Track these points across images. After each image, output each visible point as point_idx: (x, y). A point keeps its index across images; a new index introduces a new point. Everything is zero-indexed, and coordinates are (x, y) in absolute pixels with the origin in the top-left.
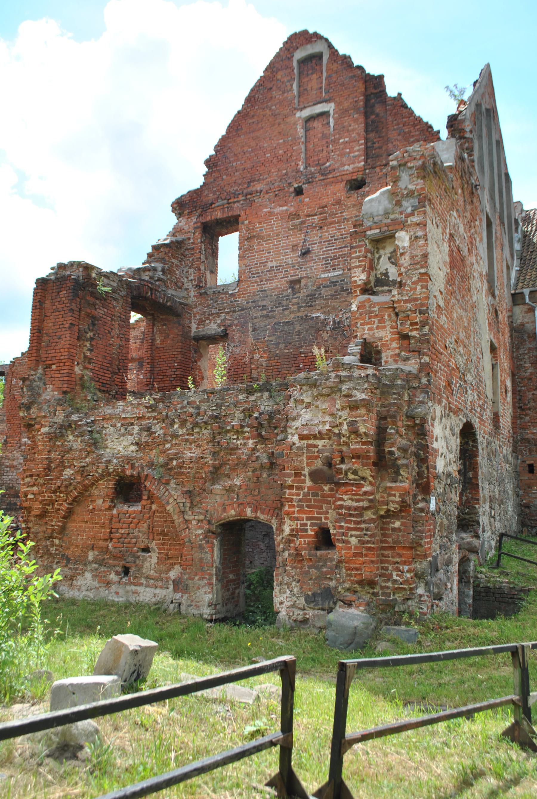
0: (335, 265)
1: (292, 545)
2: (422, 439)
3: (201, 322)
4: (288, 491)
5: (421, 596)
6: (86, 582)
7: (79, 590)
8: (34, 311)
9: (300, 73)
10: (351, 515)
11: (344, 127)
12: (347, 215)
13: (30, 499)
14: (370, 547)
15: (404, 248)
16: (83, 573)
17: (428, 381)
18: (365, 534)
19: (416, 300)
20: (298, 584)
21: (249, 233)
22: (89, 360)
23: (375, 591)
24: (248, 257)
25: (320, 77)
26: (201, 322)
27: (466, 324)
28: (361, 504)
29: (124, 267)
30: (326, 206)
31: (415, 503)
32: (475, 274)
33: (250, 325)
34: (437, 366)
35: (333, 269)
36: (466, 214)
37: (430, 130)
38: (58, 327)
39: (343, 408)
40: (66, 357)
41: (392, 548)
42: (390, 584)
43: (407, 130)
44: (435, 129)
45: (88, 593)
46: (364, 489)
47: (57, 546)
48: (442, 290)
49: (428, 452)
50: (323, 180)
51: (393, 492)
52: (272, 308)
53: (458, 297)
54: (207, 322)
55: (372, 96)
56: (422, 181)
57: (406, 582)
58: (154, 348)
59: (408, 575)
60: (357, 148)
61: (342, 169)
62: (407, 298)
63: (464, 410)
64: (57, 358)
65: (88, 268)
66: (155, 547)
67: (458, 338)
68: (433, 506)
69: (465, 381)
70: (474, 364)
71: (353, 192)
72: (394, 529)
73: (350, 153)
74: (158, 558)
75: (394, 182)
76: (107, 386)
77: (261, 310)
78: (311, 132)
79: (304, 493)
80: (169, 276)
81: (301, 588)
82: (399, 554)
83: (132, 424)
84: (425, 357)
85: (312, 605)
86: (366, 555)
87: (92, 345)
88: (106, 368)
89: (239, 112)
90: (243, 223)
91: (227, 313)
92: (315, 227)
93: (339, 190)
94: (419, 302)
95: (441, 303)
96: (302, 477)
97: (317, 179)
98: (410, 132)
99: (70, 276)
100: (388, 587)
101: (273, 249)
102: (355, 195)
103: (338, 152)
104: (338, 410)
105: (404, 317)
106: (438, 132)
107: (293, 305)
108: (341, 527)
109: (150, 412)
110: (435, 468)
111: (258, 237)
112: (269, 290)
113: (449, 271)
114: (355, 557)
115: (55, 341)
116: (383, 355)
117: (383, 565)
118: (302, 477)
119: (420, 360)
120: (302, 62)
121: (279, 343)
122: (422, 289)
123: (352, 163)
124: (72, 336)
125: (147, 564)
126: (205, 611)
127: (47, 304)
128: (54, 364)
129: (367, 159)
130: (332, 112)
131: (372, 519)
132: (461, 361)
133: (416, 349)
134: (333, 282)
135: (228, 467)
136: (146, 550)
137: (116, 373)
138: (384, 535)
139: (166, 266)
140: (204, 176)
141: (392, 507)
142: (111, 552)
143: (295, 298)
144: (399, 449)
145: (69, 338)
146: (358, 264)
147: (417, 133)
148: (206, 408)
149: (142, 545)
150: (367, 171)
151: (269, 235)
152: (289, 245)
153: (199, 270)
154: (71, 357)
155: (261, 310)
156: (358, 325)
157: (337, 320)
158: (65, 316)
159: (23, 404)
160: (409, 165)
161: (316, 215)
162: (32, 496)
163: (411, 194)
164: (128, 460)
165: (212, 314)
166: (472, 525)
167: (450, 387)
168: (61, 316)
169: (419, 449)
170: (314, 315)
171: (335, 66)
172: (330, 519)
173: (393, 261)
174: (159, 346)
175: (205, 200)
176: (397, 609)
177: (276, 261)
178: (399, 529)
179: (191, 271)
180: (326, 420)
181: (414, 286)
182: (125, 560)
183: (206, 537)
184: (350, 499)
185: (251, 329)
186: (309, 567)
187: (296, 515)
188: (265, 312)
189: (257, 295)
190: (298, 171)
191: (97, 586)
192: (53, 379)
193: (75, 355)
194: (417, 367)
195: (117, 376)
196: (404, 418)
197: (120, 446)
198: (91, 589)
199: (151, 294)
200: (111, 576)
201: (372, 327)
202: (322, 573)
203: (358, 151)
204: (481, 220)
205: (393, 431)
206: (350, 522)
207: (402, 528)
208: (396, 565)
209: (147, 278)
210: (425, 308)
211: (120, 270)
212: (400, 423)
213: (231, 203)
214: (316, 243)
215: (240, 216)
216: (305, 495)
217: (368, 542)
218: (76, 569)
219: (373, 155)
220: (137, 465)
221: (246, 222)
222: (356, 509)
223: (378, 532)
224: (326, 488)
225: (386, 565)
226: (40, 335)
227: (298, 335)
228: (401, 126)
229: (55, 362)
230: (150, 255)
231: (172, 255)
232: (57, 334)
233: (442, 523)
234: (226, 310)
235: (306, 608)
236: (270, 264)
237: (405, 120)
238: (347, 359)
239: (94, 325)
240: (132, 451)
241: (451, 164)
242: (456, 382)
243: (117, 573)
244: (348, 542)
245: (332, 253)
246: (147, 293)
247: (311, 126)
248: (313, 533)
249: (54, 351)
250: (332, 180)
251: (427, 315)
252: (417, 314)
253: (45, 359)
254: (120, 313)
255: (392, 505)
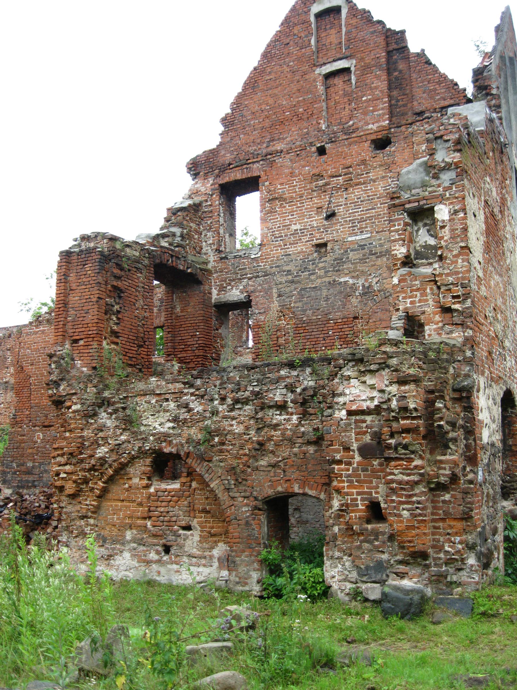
0: (362, 228)
1: (341, 520)
2: (469, 412)
3: (222, 289)
4: (336, 467)
5: (472, 566)
6: (124, 561)
7: (117, 570)
8: (59, 285)
9: (318, 28)
10: (402, 489)
11: (366, 85)
12: (373, 176)
13: (63, 478)
14: (422, 520)
15: (443, 221)
16: (121, 552)
17: (473, 354)
18: (417, 508)
19: (457, 273)
20: (349, 558)
21: (270, 195)
22: (115, 334)
23: (427, 562)
24: (270, 220)
25: (340, 31)
26: (222, 289)
27: (502, 290)
28: (412, 478)
29: (142, 234)
30: (350, 167)
31: (465, 475)
32: (507, 236)
33: (275, 290)
34: (480, 337)
35: (361, 232)
36: (497, 177)
37: (456, 87)
38: (85, 301)
39: (391, 384)
40: (95, 332)
41: (443, 520)
42: (442, 555)
43: (432, 88)
44: (461, 87)
45: (127, 573)
46: (414, 464)
47: (92, 525)
48: (481, 260)
49: (475, 425)
50: (347, 139)
51: (443, 466)
52: (297, 273)
53: (494, 264)
54: (228, 288)
55: (394, 52)
56: (459, 154)
57: (458, 552)
58: (174, 317)
59: (460, 546)
60: (381, 106)
61: (366, 127)
62: (449, 271)
63: (504, 377)
64: (85, 333)
65: (113, 239)
66: (197, 526)
67: (496, 305)
68: (480, 477)
69: (504, 348)
70: (510, 329)
71: (378, 152)
72: (444, 502)
73: (373, 111)
74: (201, 535)
75: (431, 155)
76: (134, 359)
77: (286, 275)
78: (332, 89)
79: (353, 468)
80: (187, 242)
81: (353, 562)
82: (450, 526)
83: (167, 400)
84: (468, 330)
85: (364, 579)
86: (418, 528)
87: (118, 319)
88: (132, 341)
89: (255, 69)
90: (264, 185)
91: (250, 279)
92: (340, 188)
93: (365, 150)
94: (460, 276)
95: (481, 274)
96: (351, 453)
97: (340, 139)
98: (435, 89)
99: (95, 248)
100: (440, 559)
101: (296, 211)
102: (380, 154)
103: (361, 111)
104: (387, 386)
105: (447, 290)
106: (465, 90)
107: (319, 269)
108: (393, 501)
109: (187, 388)
110: (481, 440)
111: (281, 199)
112: (294, 254)
113: (485, 239)
114: (407, 529)
115: (82, 315)
116: (426, 328)
117: (435, 537)
118: (351, 453)
119: (464, 333)
120: (319, 15)
121: (306, 310)
122: (463, 262)
123: (377, 122)
124: (100, 310)
125: (188, 542)
126: (255, 588)
127: (72, 277)
128: (82, 339)
129: (392, 117)
130: (353, 69)
131: (424, 492)
132: (499, 327)
133: (459, 323)
134: (361, 246)
135: (273, 443)
136: (188, 528)
137: (141, 346)
138: (434, 508)
139: (185, 231)
140: (221, 134)
141: (442, 479)
142: (150, 531)
143: (322, 262)
144: (447, 423)
146: (397, 237)
147: (442, 91)
148: (246, 383)
149: (183, 523)
150: (393, 130)
151: (292, 197)
152: (313, 207)
153: (219, 233)
154: (100, 332)
155: (286, 275)
156: (400, 298)
157: (367, 285)
158: (91, 289)
160: (445, 138)
161: (340, 176)
162: (65, 475)
163: (448, 167)
164: (165, 437)
165: (234, 280)
166: (513, 493)
167: (491, 356)
169: (466, 422)
170: (342, 280)
171: (354, 21)
172: (380, 494)
173: (432, 233)
174: (179, 315)
175: (221, 160)
176: (449, 579)
177: (300, 223)
178: (450, 501)
179: (209, 234)
180: (374, 395)
181: (455, 259)
182: (165, 538)
183: (252, 514)
184: (401, 473)
185: (275, 295)
186: (361, 542)
187: (346, 490)
188: (290, 277)
189: (281, 259)
190: (320, 130)
191: (137, 565)
192: (81, 355)
193: (102, 329)
194: (460, 340)
195: (142, 349)
196: (450, 391)
197: (157, 423)
198: (131, 569)
199: (172, 261)
200: (151, 555)
201: (415, 301)
202: (375, 546)
203: (382, 109)
204: (511, 178)
205: (441, 405)
206: (401, 496)
207: (452, 500)
208: (448, 537)
209: (166, 245)
210: (467, 282)
211: (138, 237)
212: (447, 398)
213: (250, 163)
214: (341, 205)
215: (259, 177)
216: (354, 470)
217: (420, 515)
218: (114, 549)
219: (398, 113)
220: (174, 442)
221: (267, 183)
222: (407, 483)
223: (429, 505)
224: (375, 463)
225: (437, 537)
226: (66, 309)
227: (326, 301)
228: (426, 83)
229: (83, 337)
230: (167, 220)
231: (190, 219)
233: (488, 493)
234: (249, 276)
235: (358, 581)
236: (294, 227)
237: (430, 77)
238: (392, 334)
239: (120, 297)
240: (169, 428)
241: (483, 128)
242: (496, 350)
243: (158, 553)
244: (400, 516)
245: (359, 215)
246: (168, 261)
247: (332, 83)
248: (364, 507)
250: (356, 139)
251: (469, 288)
252: (459, 287)
253: (72, 334)
254: (144, 283)
255: (442, 478)
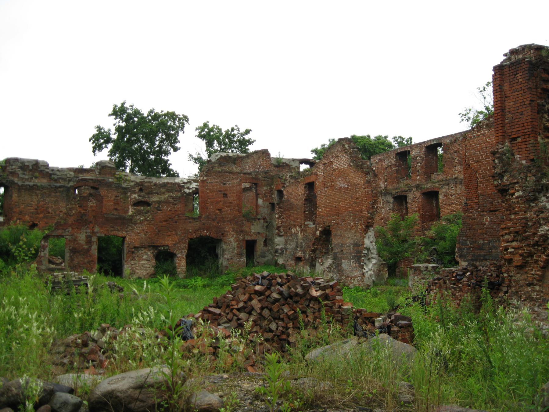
8: (496, 94)
13: (511, 252)
38: (519, 105)
40: (530, 130)
47: (538, 291)
64: (521, 132)
99: (524, 59)
115: (518, 117)
127: (506, 86)
145: (531, 113)
154: (534, 129)
158: (524, 94)
159: (496, 173)
162: (513, 250)
168: (520, 95)
192: (520, 150)
193: (536, 127)
229: (520, 135)
232: (519, 111)
249: (517, 126)
253: (510, 134)
